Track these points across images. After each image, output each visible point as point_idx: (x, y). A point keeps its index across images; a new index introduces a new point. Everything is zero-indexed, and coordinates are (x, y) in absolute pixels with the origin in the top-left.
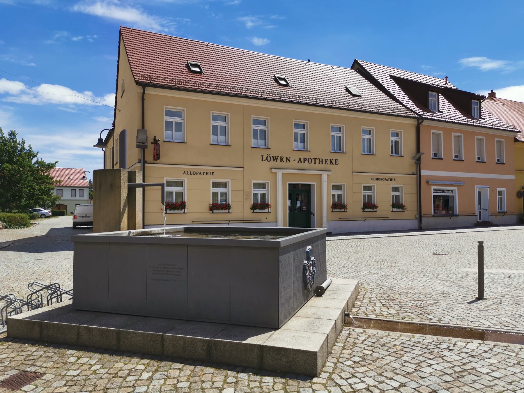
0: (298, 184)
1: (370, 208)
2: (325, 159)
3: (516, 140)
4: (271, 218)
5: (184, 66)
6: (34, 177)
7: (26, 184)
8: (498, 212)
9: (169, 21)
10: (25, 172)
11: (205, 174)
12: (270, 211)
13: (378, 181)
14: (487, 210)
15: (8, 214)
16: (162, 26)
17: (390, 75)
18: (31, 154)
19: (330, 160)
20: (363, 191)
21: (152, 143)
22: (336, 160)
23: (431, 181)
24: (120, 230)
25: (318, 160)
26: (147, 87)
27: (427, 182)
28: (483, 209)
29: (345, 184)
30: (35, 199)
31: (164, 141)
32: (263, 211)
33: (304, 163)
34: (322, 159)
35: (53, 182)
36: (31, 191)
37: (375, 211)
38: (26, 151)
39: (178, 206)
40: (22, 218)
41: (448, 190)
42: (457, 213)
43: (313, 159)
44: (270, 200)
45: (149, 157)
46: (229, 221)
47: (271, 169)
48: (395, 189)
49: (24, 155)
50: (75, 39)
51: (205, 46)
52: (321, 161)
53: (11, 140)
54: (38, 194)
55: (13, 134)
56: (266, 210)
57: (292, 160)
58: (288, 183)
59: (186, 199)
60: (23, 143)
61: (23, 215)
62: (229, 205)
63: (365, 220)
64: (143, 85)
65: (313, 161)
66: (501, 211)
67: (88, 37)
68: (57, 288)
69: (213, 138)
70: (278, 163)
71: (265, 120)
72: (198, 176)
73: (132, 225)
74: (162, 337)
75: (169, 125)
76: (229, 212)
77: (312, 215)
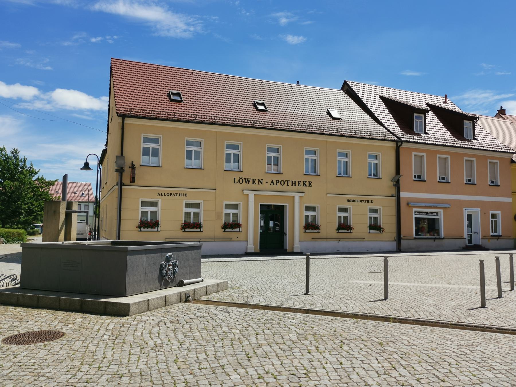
0: (271, 205)
1: (345, 229)
2: (298, 182)
3: (512, 161)
4: (242, 237)
5: (166, 95)
6: (34, 193)
7: (25, 201)
8: (491, 236)
9: (195, 19)
10: (25, 189)
11: (178, 195)
12: (241, 231)
13: (354, 203)
14: (478, 233)
15: (7, 229)
16: (188, 24)
17: (380, 96)
18: (32, 172)
19: (304, 182)
20: (337, 213)
21: (130, 167)
22: (309, 182)
23: (411, 203)
24: (58, 241)
25: (291, 182)
26: (126, 118)
27: (408, 204)
28: (475, 233)
29: (319, 205)
30: (34, 215)
31: (141, 166)
32: (153, 230)
33: (277, 185)
34: (295, 181)
35: (52, 198)
36: (31, 208)
37: (350, 232)
38: (27, 168)
39: (152, 225)
40: (19, 234)
41: (432, 213)
42: (443, 236)
43: (286, 181)
44: (241, 221)
45: (126, 179)
46: (200, 239)
47: (243, 190)
48: (375, 211)
49: (25, 172)
50: (93, 40)
51: (190, 73)
52: (294, 183)
53: (14, 158)
54: (36, 210)
55: (15, 152)
56: (237, 230)
57: (264, 182)
58: (260, 204)
59: (159, 218)
60: (25, 160)
61: (22, 231)
62: (201, 224)
63: (339, 241)
64: (123, 116)
65: (286, 183)
66: (496, 234)
67: (108, 37)
68: (14, 277)
69: (187, 163)
70: (250, 185)
71: (238, 144)
72: (172, 197)
73: (67, 237)
74: (60, 298)
75: (146, 152)
76: (200, 231)
77: (284, 235)
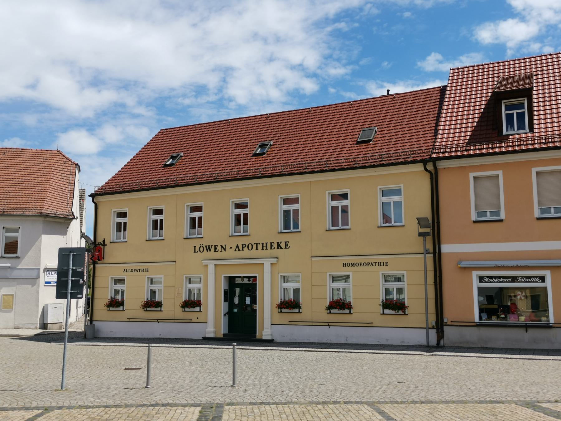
11: (377, 264)
12: (300, 312)
19: (278, 243)
22: (286, 242)
25: (261, 244)
26: (437, 162)
32: (117, 309)
41: (491, 278)
43: (254, 244)
52: (264, 246)
57: (227, 248)
65: (255, 246)
70: (212, 254)
72: (135, 273)
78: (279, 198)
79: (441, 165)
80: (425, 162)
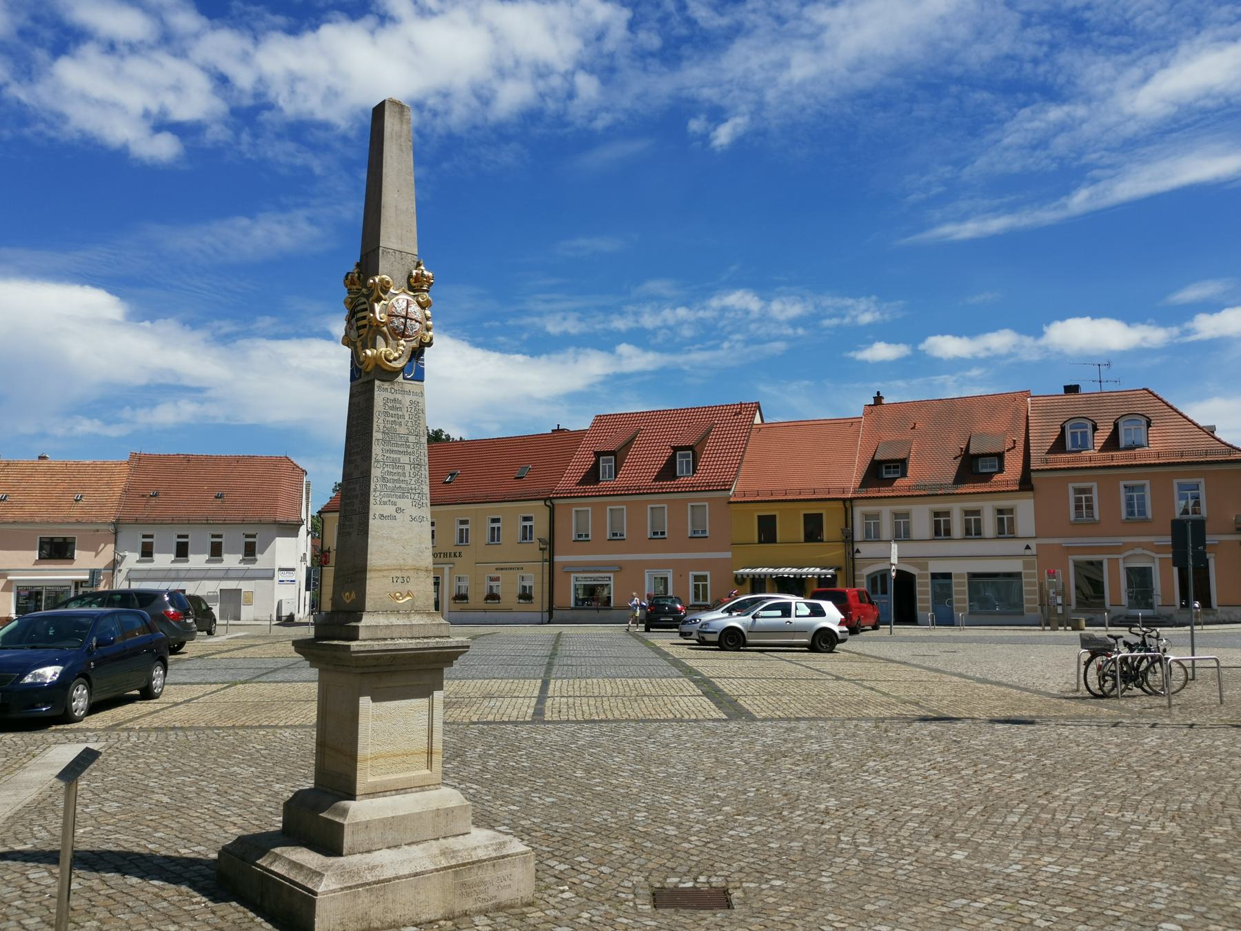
52: (445, 555)
78: (574, 512)
79: (556, 502)
80: (545, 500)
